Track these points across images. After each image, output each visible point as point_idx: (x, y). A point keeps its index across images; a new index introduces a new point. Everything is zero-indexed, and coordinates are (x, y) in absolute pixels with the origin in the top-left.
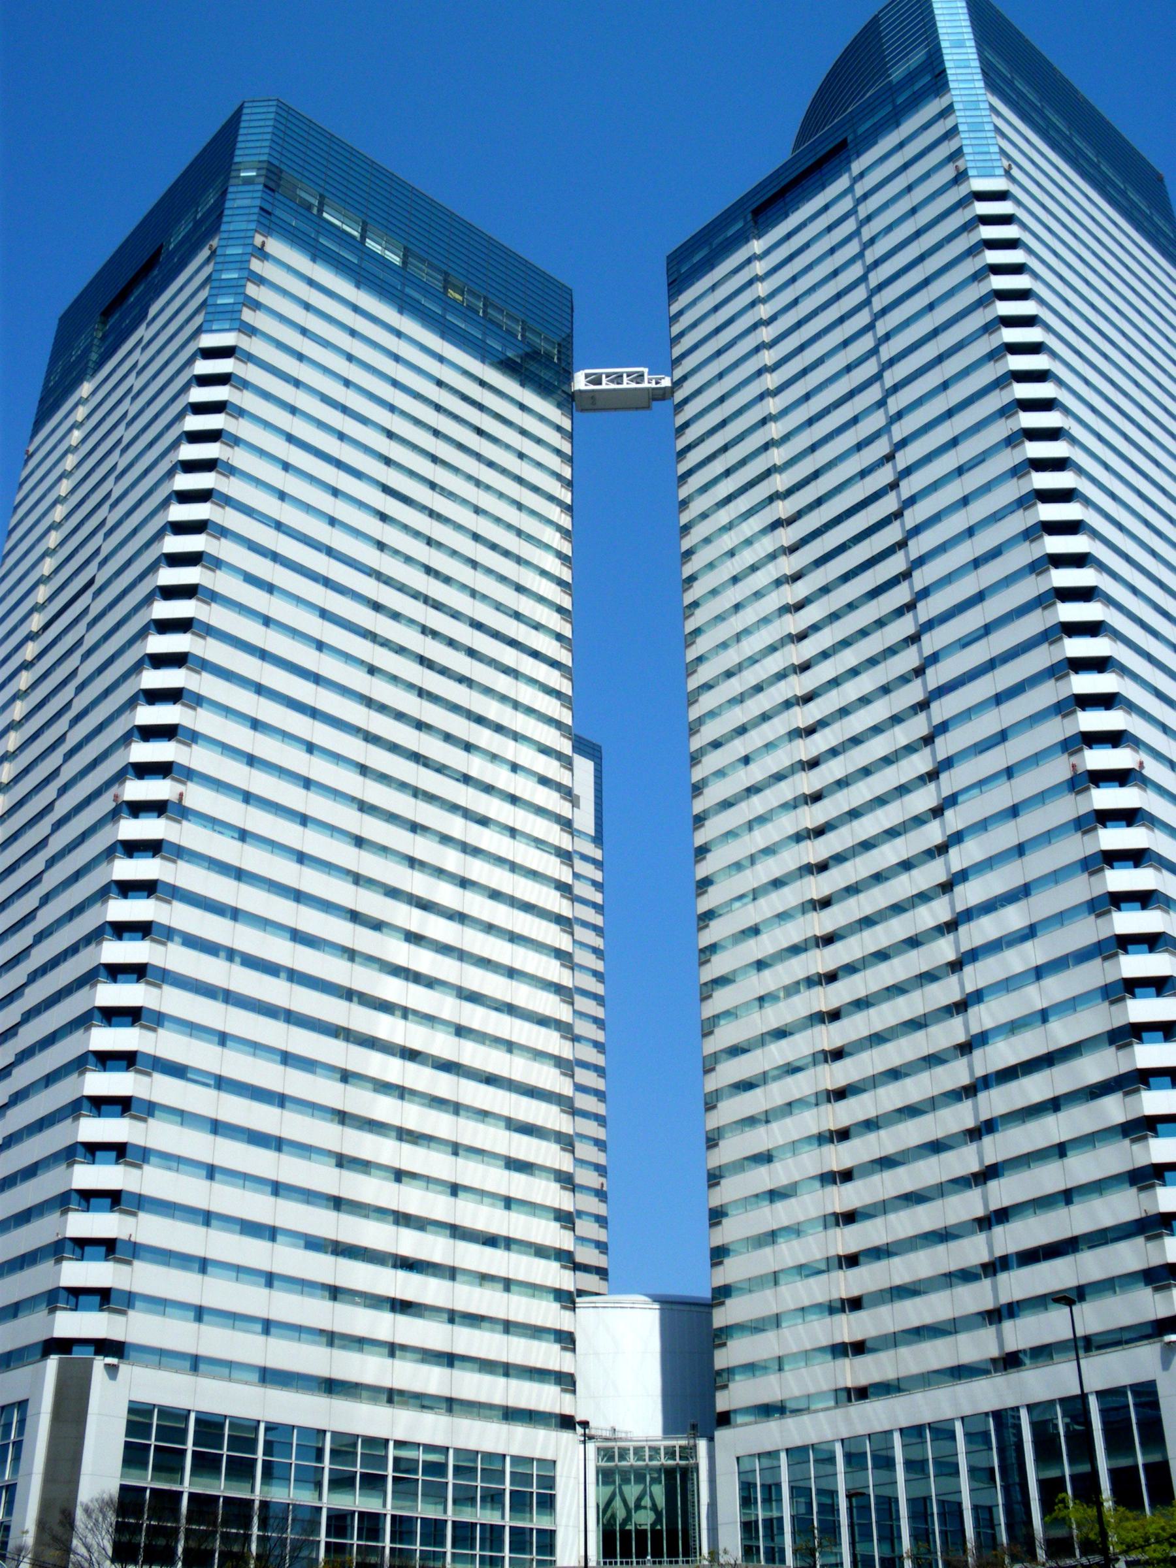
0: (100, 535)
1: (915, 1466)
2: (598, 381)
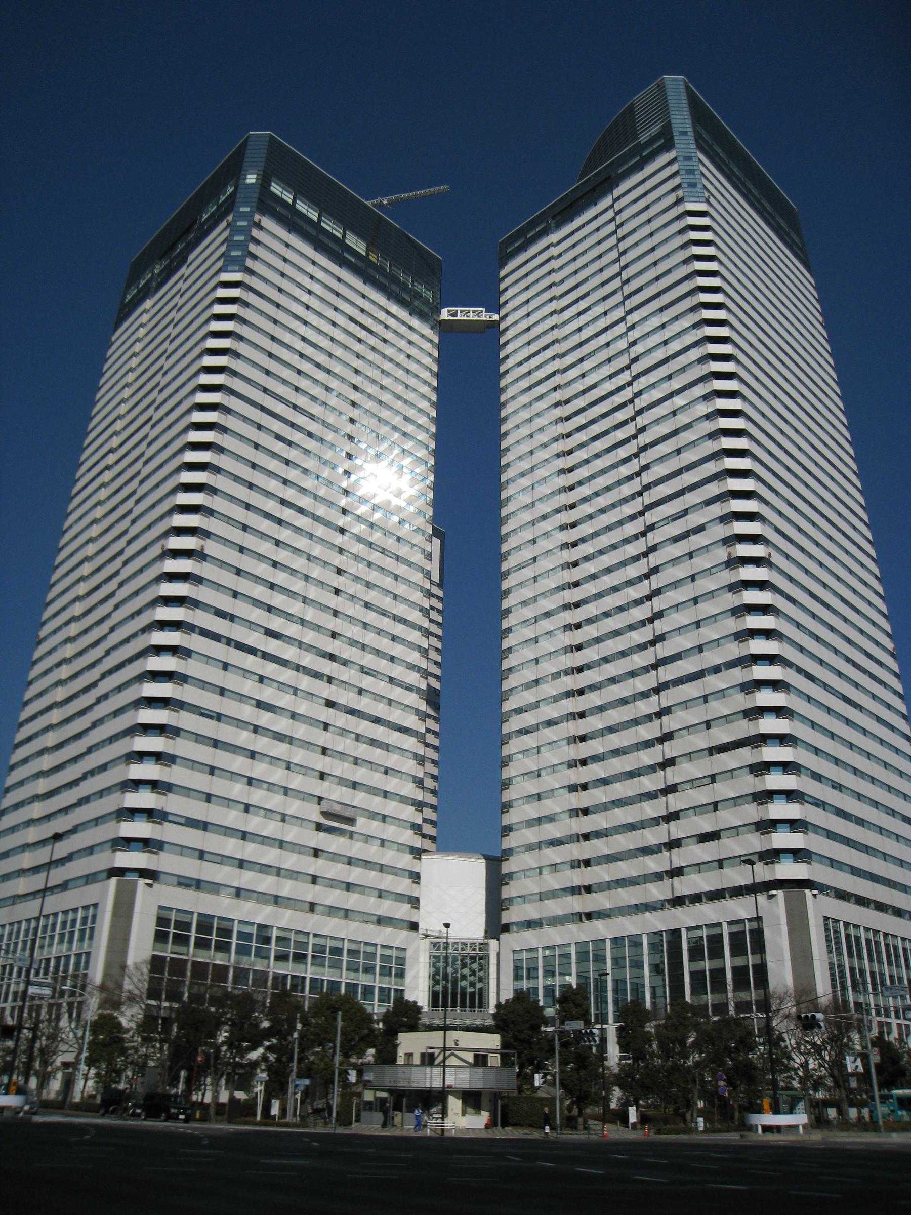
0: (156, 391)
1: (618, 962)
2: (455, 315)
